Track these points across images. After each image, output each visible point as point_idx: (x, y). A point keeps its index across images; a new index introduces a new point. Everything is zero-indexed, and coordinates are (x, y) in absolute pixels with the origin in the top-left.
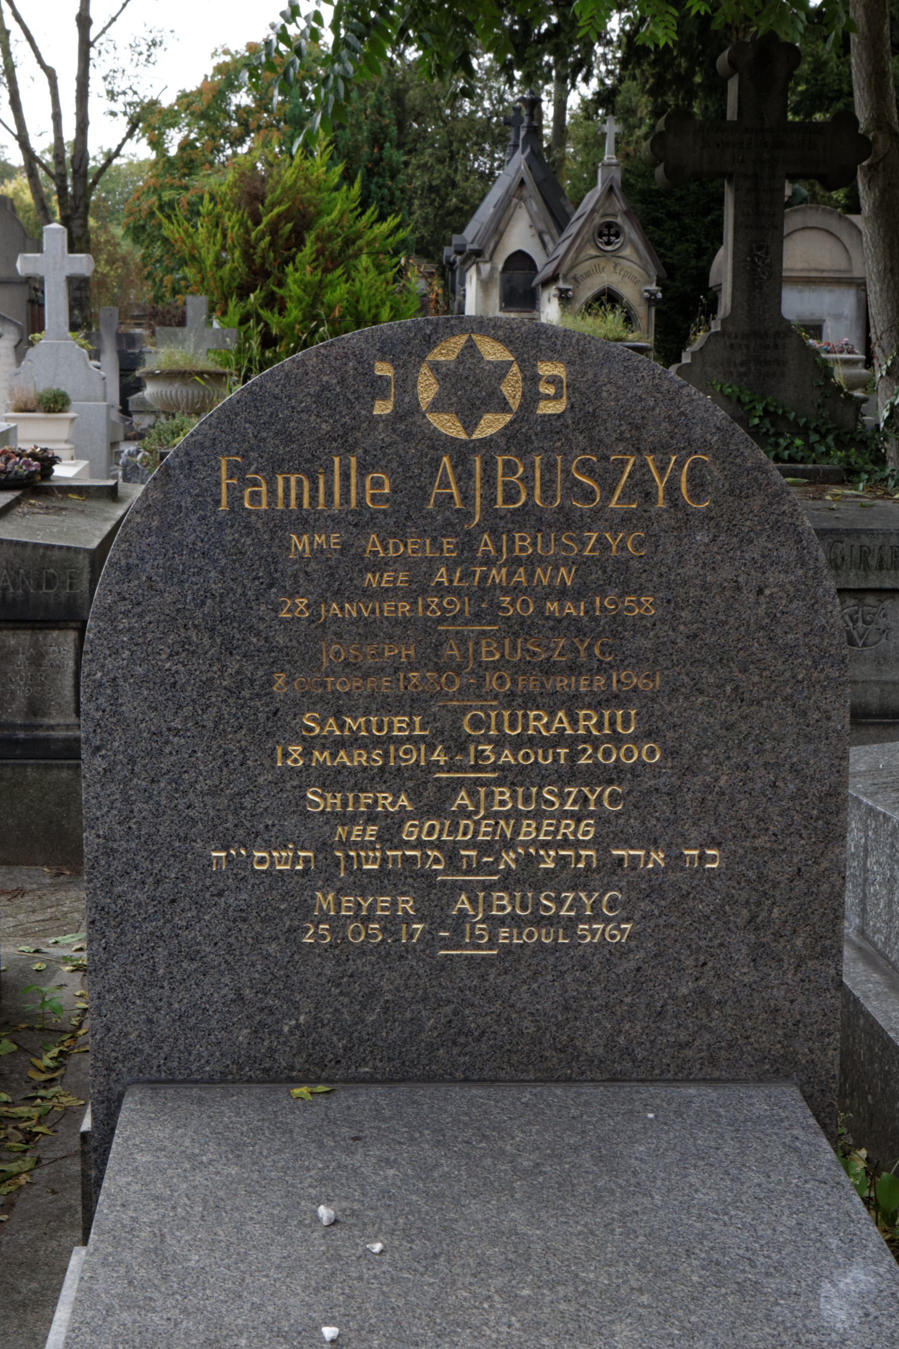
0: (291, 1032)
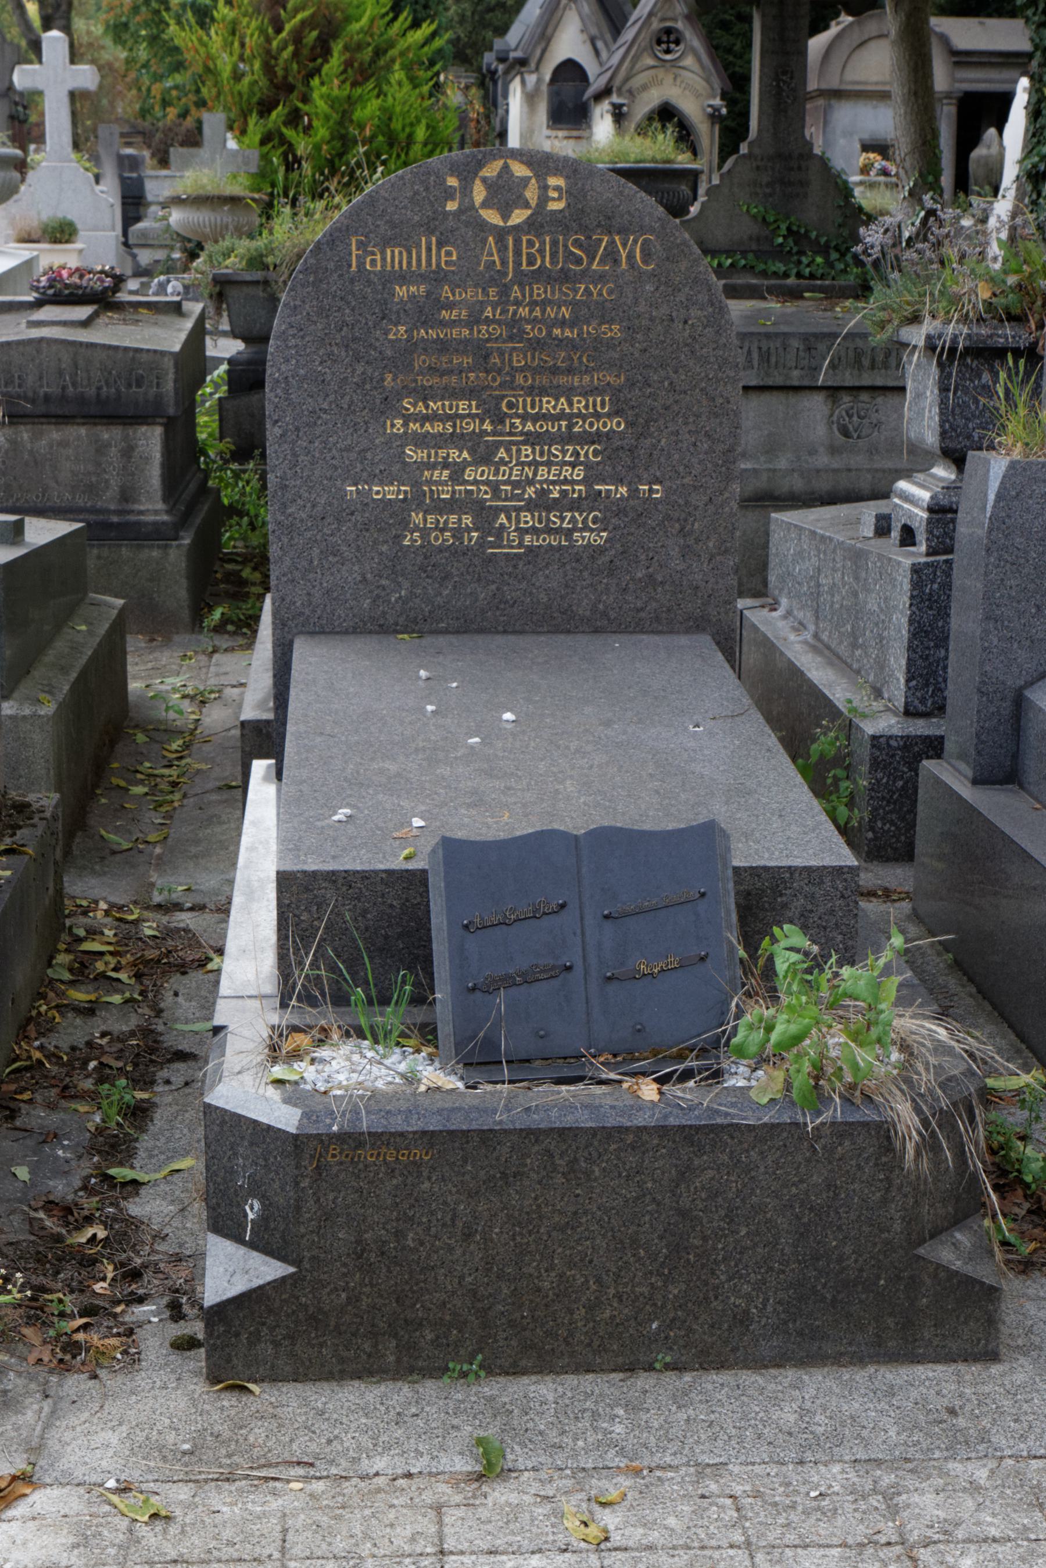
0: (396, 601)
